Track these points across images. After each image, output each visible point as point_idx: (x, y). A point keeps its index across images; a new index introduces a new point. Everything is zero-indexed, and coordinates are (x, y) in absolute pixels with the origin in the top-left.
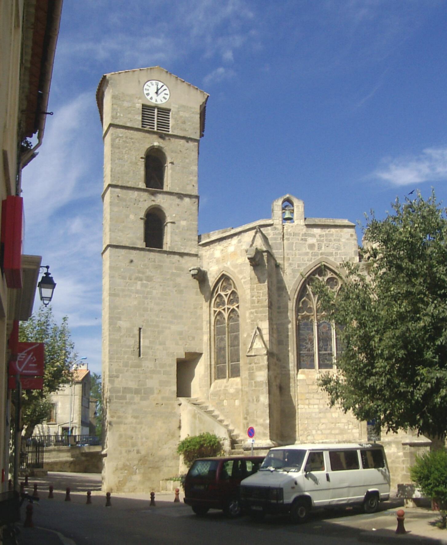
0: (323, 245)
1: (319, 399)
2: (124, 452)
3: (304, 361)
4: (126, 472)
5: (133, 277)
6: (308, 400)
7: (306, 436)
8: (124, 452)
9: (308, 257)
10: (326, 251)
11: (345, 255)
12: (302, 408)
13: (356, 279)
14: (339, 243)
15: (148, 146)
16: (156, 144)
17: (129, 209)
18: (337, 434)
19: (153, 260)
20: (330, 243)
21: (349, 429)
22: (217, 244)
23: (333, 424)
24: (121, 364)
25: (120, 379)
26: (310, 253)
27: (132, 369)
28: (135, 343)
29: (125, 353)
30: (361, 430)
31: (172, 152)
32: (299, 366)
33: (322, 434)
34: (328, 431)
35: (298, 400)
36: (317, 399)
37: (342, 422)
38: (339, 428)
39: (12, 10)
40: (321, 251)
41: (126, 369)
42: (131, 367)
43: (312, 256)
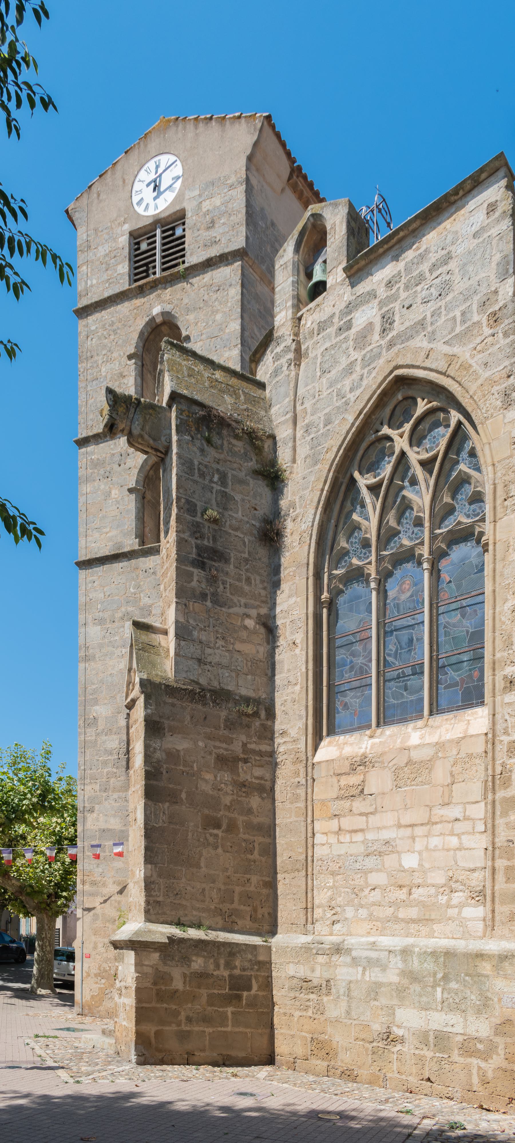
1: (366, 815)
2: (100, 945)
3: (346, 706)
4: (103, 981)
5: (119, 615)
6: (336, 821)
7: (328, 922)
8: (100, 945)
12: (323, 845)
15: (140, 323)
16: (156, 310)
17: (109, 479)
18: (413, 921)
19: (152, 571)
21: (452, 907)
23: (405, 890)
24: (97, 787)
25: (95, 815)
27: (116, 795)
28: (119, 744)
29: (105, 763)
30: (493, 911)
32: (328, 735)
33: (371, 918)
34: (390, 911)
35: (313, 821)
36: (361, 814)
37: (430, 881)
38: (422, 905)
41: (105, 794)
42: (113, 791)
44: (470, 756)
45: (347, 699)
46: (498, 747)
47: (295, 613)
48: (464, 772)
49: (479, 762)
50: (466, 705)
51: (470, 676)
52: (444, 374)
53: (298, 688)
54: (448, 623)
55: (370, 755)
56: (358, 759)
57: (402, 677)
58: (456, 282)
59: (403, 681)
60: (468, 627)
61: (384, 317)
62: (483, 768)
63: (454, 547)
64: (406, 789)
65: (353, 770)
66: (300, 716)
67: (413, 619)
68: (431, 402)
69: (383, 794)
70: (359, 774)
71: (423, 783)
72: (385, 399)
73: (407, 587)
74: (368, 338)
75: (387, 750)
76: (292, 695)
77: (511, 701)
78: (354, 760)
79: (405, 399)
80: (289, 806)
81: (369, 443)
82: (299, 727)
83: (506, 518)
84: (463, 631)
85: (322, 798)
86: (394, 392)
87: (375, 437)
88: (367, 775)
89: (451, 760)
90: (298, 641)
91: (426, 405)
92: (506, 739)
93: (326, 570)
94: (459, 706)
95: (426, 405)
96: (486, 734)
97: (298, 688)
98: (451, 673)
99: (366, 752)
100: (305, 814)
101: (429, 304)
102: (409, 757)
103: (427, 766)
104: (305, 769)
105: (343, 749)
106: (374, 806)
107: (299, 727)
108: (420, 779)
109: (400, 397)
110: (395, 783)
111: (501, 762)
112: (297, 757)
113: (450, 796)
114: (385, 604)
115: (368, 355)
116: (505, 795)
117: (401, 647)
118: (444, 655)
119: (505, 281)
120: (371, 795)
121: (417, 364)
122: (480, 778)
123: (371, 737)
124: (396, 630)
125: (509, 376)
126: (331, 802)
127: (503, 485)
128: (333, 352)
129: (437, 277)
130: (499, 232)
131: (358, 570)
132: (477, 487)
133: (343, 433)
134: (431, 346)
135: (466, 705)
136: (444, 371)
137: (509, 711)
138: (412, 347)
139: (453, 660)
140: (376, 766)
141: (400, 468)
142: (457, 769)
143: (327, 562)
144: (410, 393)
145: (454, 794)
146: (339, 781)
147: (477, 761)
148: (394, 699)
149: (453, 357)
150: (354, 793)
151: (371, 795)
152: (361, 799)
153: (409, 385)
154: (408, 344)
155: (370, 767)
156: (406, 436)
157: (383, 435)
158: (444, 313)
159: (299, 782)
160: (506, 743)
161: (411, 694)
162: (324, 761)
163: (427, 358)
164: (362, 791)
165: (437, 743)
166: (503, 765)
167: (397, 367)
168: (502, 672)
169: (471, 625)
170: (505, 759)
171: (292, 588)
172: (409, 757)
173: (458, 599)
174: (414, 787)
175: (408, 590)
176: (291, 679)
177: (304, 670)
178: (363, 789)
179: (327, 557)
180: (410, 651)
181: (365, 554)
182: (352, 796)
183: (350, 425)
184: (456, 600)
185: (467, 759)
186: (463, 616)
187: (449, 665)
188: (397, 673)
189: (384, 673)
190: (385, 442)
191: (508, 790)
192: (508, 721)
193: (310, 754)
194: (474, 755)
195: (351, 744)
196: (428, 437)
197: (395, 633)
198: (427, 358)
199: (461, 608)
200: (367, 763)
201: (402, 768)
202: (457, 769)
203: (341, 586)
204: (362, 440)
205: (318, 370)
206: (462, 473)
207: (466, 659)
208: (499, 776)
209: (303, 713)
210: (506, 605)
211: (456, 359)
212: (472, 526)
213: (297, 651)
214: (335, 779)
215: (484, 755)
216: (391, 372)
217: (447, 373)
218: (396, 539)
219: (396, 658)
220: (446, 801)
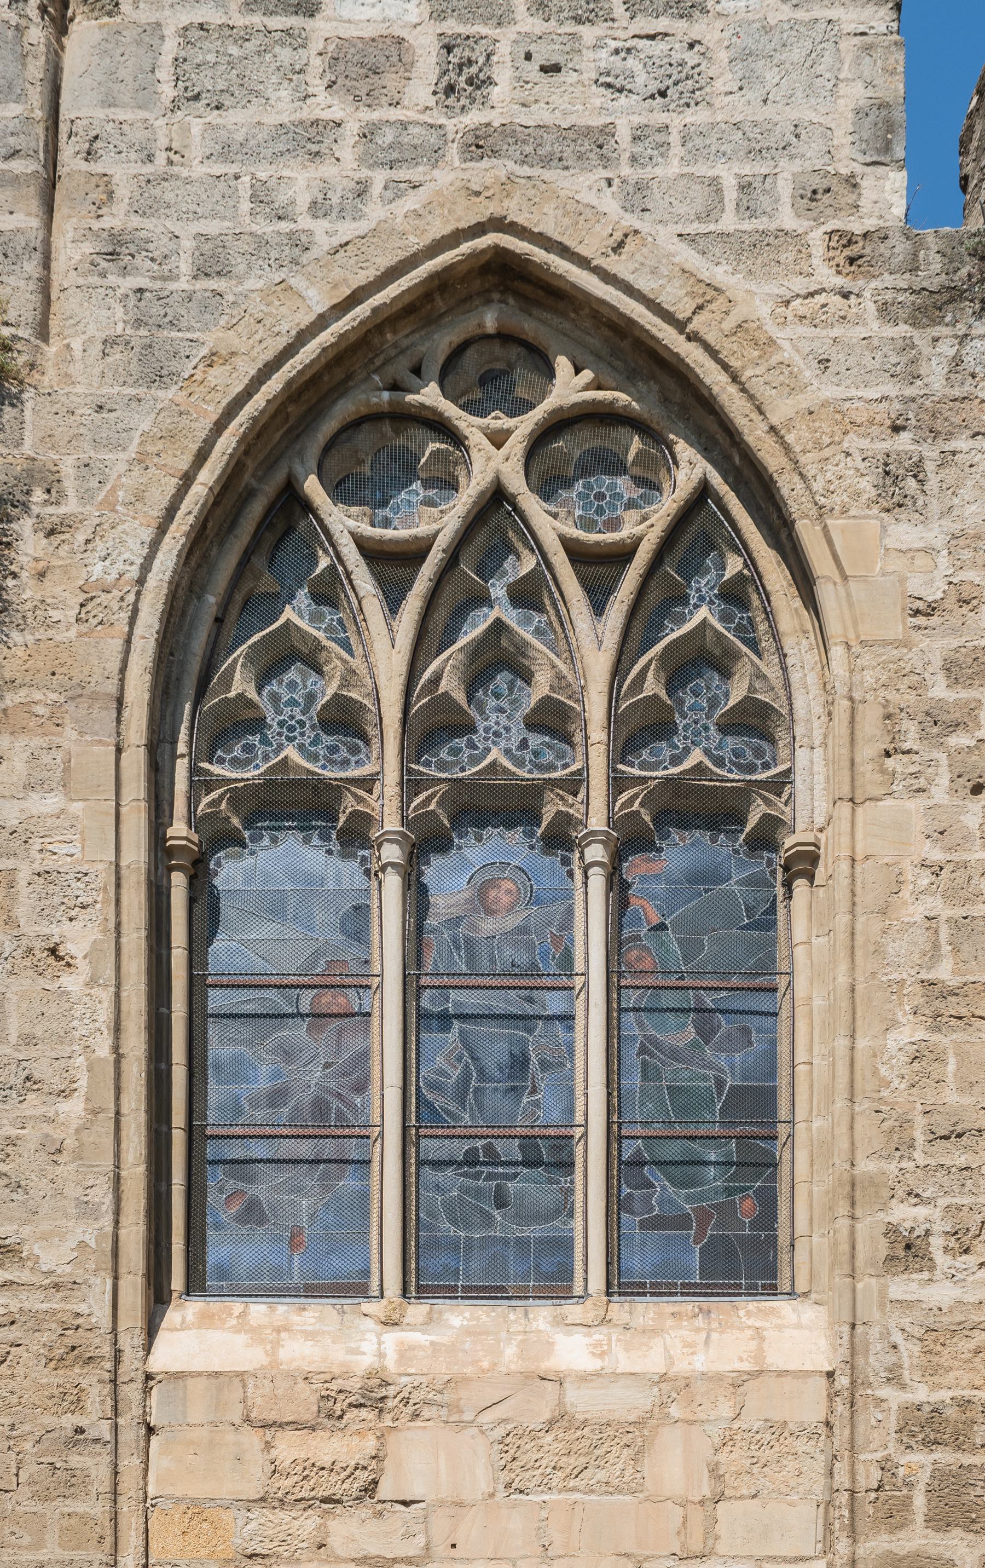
0: (503, 49)
9: (327, 170)
10: (539, 115)
11: (754, 153)
13: (553, 206)
14: (679, 26)
20: (588, 33)
22: (112, 1016)
26: (352, 129)
31: (618, 248)
32: (189, 1290)
39: (586, 943)
40: (474, 118)
43: (365, 160)
44: (778, 1428)
45: (259, 1190)
46: (869, 1416)
47: (63, 849)
48: (756, 1469)
49: (807, 1448)
50: (708, 1286)
51: (727, 1212)
52: (680, 326)
53: (74, 1108)
54: (653, 1041)
55: (404, 1380)
56: (354, 1385)
57: (484, 1164)
58: (719, 85)
59: (490, 1177)
60: (721, 1070)
61: (449, 49)
62: (820, 1464)
63: (675, 835)
64: (545, 1497)
65: (329, 1416)
66: (87, 1210)
67: (530, 1000)
68: (599, 388)
69: (460, 1504)
70: (358, 1432)
71: (609, 1488)
72: (440, 304)
73: (505, 900)
74: (390, 80)
75: (469, 1370)
76: (47, 1128)
77: (909, 1297)
78: (335, 1386)
79: (504, 337)
80: (30, 1506)
81: (364, 410)
82: (82, 1245)
83: (889, 802)
84: (705, 1078)
85: (192, 1493)
86: (469, 298)
87: (390, 402)
88: (391, 1439)
89: (716, 1432)
90: (74, 948)
91: (587, 388)
92: (894, 1397)
93: (182, 748)
94: (695, 1285)
95: (587, 388)
96: (830, 1375)
97: (74, 1108)
98: (664, 1188)
99: (384, 1368)
100: (109, 1540)
101: (623, 100)
102: (560, 1403)
103: (627, 1439)
104: (108, 1388)
105: (277, 1344)
106: (421, 1540)
107: (82, 1245)
108: (601, 1475)
109: (490, 320)
110: (504, 1477)
111: (879, 1455)
112: (69, 1342)
113: (710, 1533)
114: (420, 928)
115: (387, 136)
116: (892, 1547)
117: (481, 1071)
118: (638, 1130)
119: (881, 169)
120: (406, 1503)
121: (582, 250)
122: (810, 1492)
123: (390, 1323)
124: (462, 1017)
125: (896, 429)
126: (232, 1513)
127: (880, 712)
128: (234, 50)
129: (652, 37)
130: (862, 29)
131: (315, 788)
132: (755, 691)
133: (284, 327)
134: (630, 221)
135: (708, 1286)
136: (680, 316)
137: (905, 1322)
138: (563, 193)
139: (672, 1151)
140: (426, 1413)
141: (480, 539)
142: (730, 1460)
143: (185, 725)
144: (529, 327)
145: (720, 1529)
146: (268, 1446)
147: (801, 1445)
148: (454, 1223)
149: (711, 293)
150: (338, 1491)
151: (406, 1503)
152: (364, 1511)
153: (528, 303)
154: (548, 175)
155: (404, 1419)
156: (516, 446)
157: (423, 406)
158: (677, 150)
159: (80, 1430)
160: (895, 1407)
161: (522, 1218)
162: (199, 1374)
163: (614, 250)
164: (371, 1488)
165: (663, 1377)
166: (885, 1466)
167: (498, 224)
168: (881, 1215)
169: (732, 1067)
170: (891, 1450)
171: (46, 759)
172: (560, 1403)
173: (688, 982)
174: (577, 1496)
175: (510, 909)
176: (41, 1070)
177: (104, 1050)
178: (375, 1482)
179: (188, 707)
180: (515, 1091)
181: (333, 749)
182: (325, 1500)
183: (311, 317)
184: (681, 983)
185: (768, 1437)
186: (706, 1033)
187: (656, 1163)
188: (467, 1145)
189: (418, 1136)
190: (420, 433)
191: (902, 1534)
192: (902, 1348)
193: (130, 1341)
194: (792, 1426)
195: (310, 1335)
196: (579, 486)
197: (456, 1024)
198: (614, 250)
199: (697, 1010)
200: (390, 1403)
201: (533, 1435)
202: (730, 1460)
203: (236, 821)
204: (341, 389)
205: (165, 74)
206: (709, 633)
207: (713, 1158)
208: (873, 1495)
209: (102, 1195)
210: (892, 1035)
211: (719, 304)
212: (745, 793)
213: (72, 982)
214: (252, 1439)
215: (822, 1430)
216: (479, 229)
217: (690, 328)
218: (461, 742)
219: (462, 1101)
220: (696, 1546)
